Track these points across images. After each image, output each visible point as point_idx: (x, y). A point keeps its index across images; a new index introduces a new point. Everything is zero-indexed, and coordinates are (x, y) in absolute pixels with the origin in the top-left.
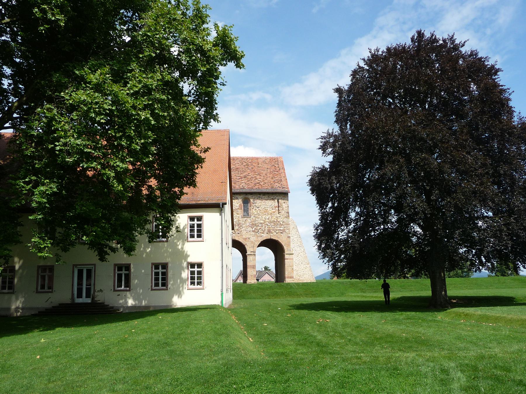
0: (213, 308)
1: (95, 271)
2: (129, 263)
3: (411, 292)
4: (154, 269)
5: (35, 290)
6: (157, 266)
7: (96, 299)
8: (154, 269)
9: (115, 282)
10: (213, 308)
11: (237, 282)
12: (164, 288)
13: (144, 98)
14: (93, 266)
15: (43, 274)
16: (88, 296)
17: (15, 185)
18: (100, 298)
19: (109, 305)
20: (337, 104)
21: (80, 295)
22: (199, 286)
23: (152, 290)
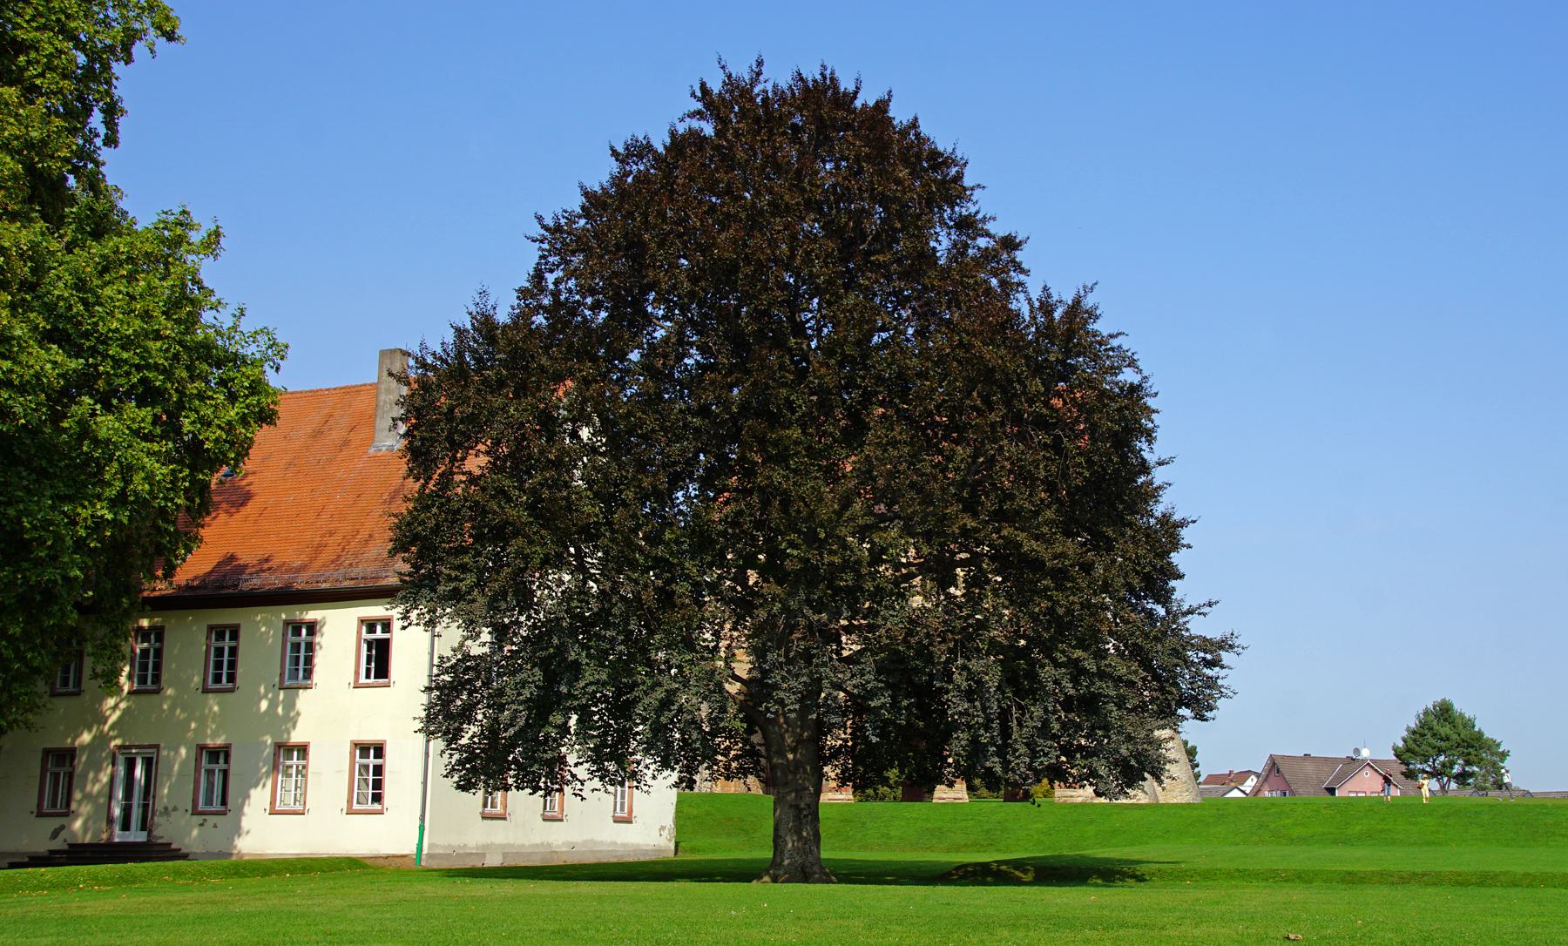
0: (1148, 862)
1: (157, 763)
2: (306, 740)
3: (984, 854)
4: (357, 758)
5: (345, 806)
6: (363, 748)
7: (155, 833)
8: (357, 758)
9: (57, 796)
10: (1148, 862)
11: (1260, 795)
12: (377, 806)
13: (649, 320)
14: (155, 750)
15: (56, 770)
16: (143, 828)
17: (850, 608)
18: (165, 830)
19: (180, 850)
20: (882, 106)
21: (126, 826)
22: (522, 803)
23: (350, 812)
